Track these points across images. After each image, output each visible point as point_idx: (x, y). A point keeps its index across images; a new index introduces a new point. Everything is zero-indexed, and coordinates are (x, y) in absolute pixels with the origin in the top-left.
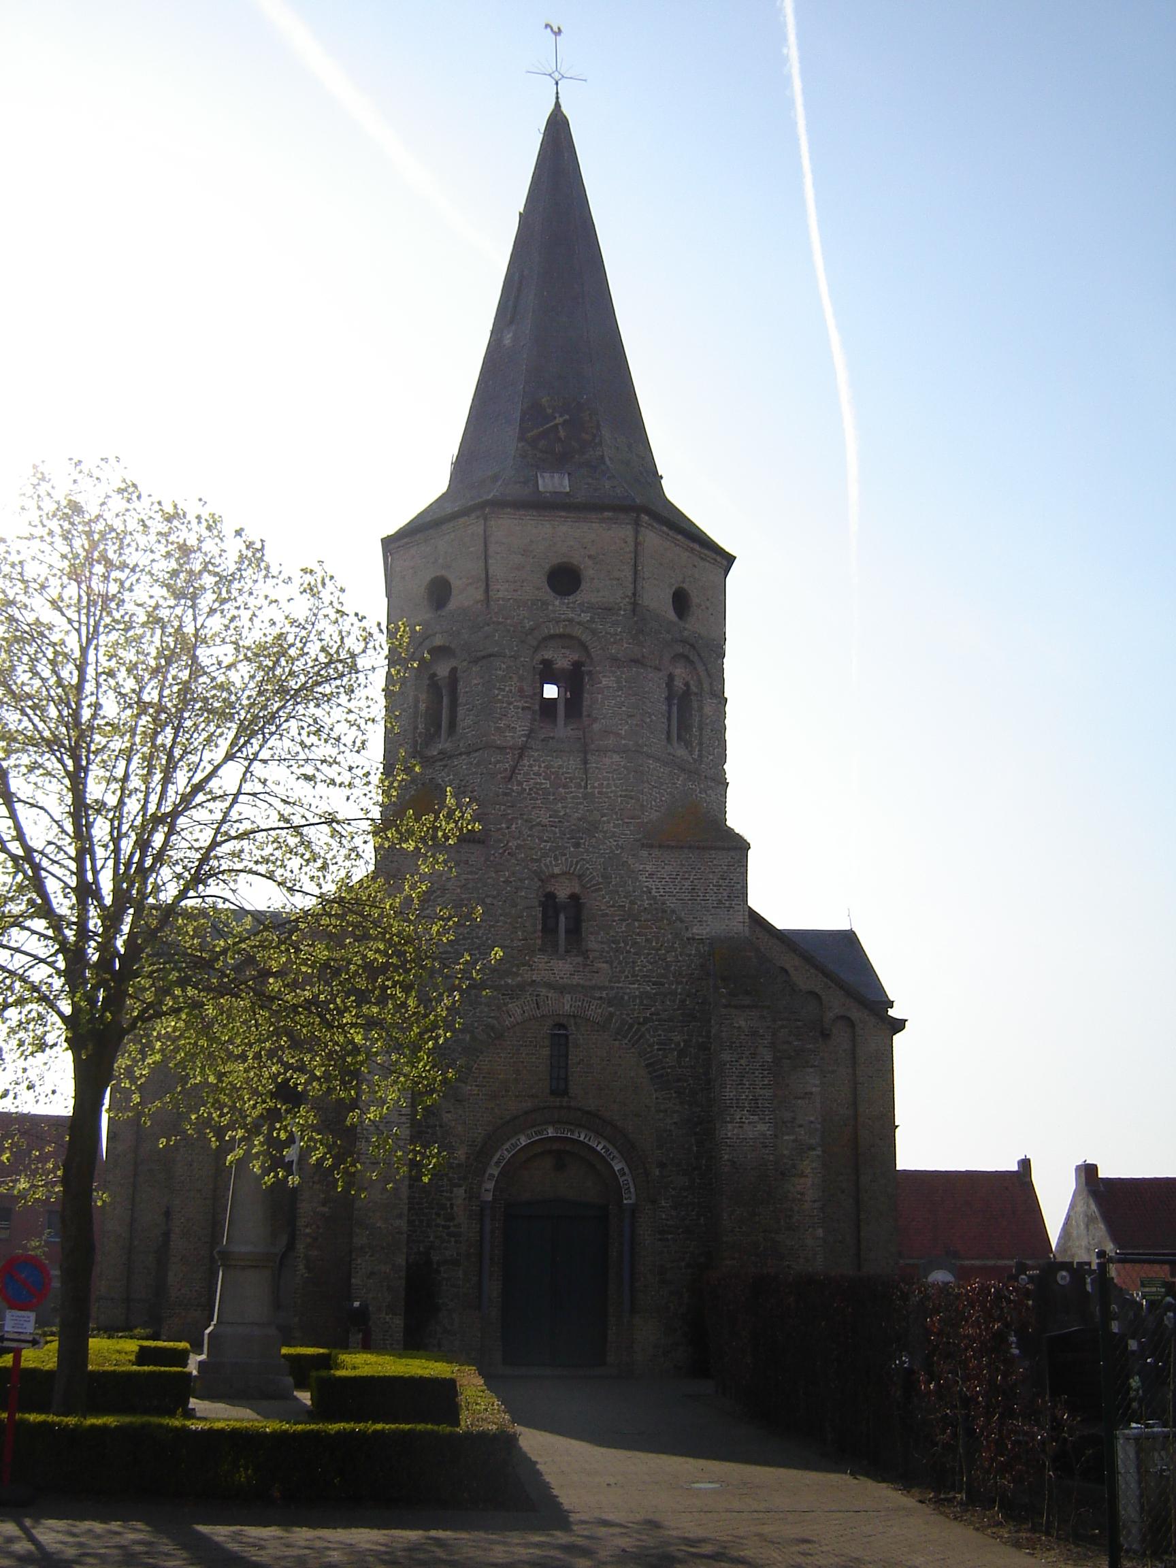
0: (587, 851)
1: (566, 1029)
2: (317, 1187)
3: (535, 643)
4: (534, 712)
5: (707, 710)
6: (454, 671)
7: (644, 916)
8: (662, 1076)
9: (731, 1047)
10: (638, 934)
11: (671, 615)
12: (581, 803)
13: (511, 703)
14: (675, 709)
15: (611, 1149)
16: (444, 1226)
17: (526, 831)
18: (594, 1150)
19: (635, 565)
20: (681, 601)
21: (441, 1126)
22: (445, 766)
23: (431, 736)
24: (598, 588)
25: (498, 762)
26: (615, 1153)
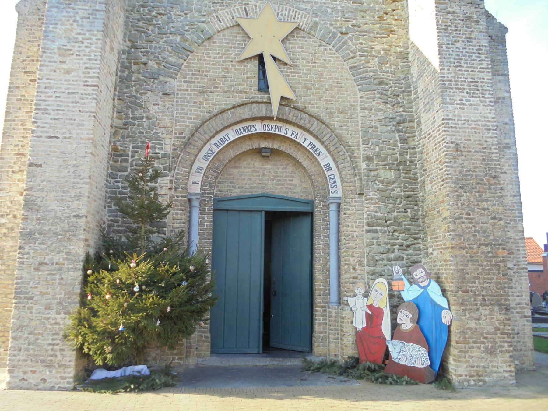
21: (148, 118)
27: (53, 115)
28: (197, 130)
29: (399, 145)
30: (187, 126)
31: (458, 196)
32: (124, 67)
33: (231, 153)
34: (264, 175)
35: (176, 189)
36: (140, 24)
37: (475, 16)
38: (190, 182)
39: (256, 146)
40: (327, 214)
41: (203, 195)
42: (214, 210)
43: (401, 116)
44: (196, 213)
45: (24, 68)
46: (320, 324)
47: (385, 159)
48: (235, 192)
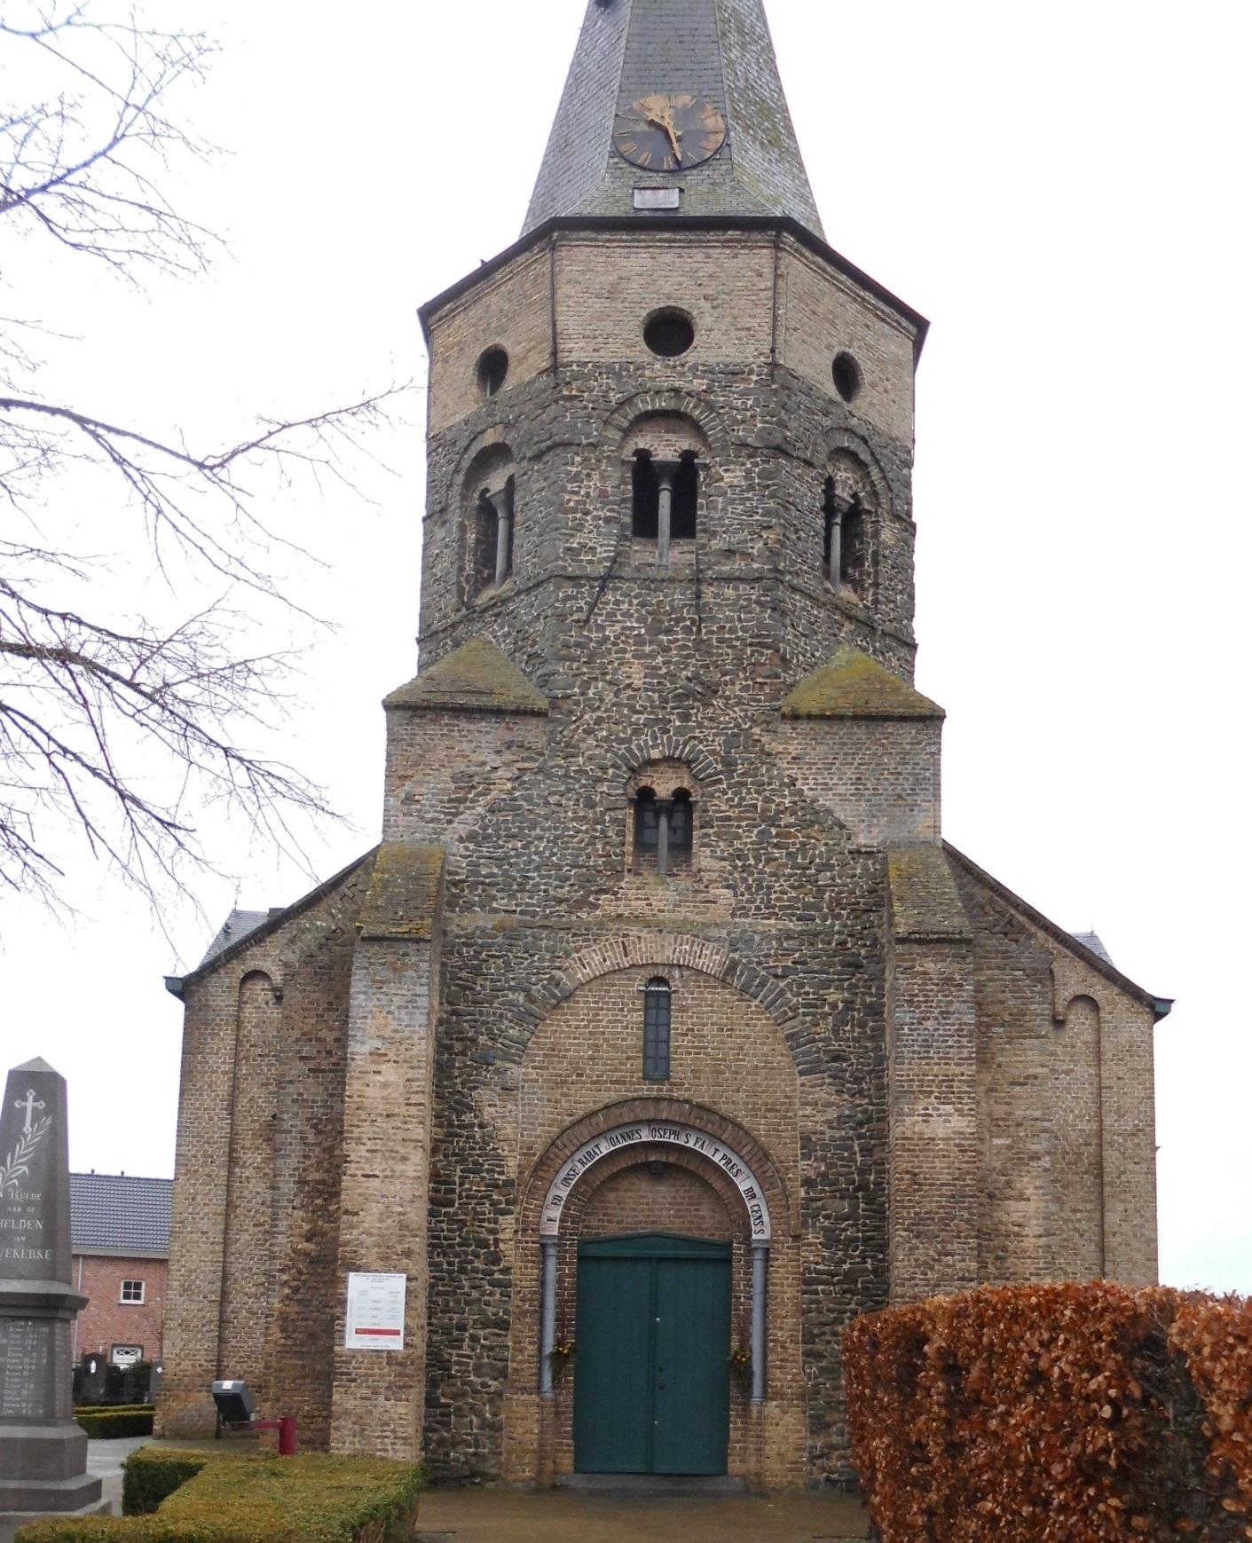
0: (700, 726)
1: (666, 983)
2: (298, 1214)
3: (626, 424)
4: (623, 526)
5: (886, 536)
6: (511, 480)
7: (787, 819)
8: (808, 1053)
9: (910, 1002)
10: (776, 846)
11: (831, 390)
12: (693, 656)
13: (586, 513)
14: (837, 531)
15: (735, 1159)
16: (484, 1272)
17: (610, 698)
18: (707, 1161)
19: (775, 308)
20: (846, 373)
21: (481, 1126)
22: (498, 615)
23: (484, 578)
24: (714, 344)
25: (567, 598)
26: (741, 1166)
27: (370, 1145)
28: (553, 1143)
29: (859, 1159)
30: (540, 1136)
31: (911, 1249)
32: (442, 1047)
33: (606, 1172)
34: (655, 1203)
35: (525, 1230)
36: (463, 974)
37: (957, 977)
38: (544, 1219)
39: (641, 1159)
40: (749, 1264)
41: (562, 1236)
42: (579, 1258)
43: (865, 1112)
44: (551, 1264)
45: (299, 1052)
46: (736, 1429)
47: (836, 1182)
48: (612, 1230)
